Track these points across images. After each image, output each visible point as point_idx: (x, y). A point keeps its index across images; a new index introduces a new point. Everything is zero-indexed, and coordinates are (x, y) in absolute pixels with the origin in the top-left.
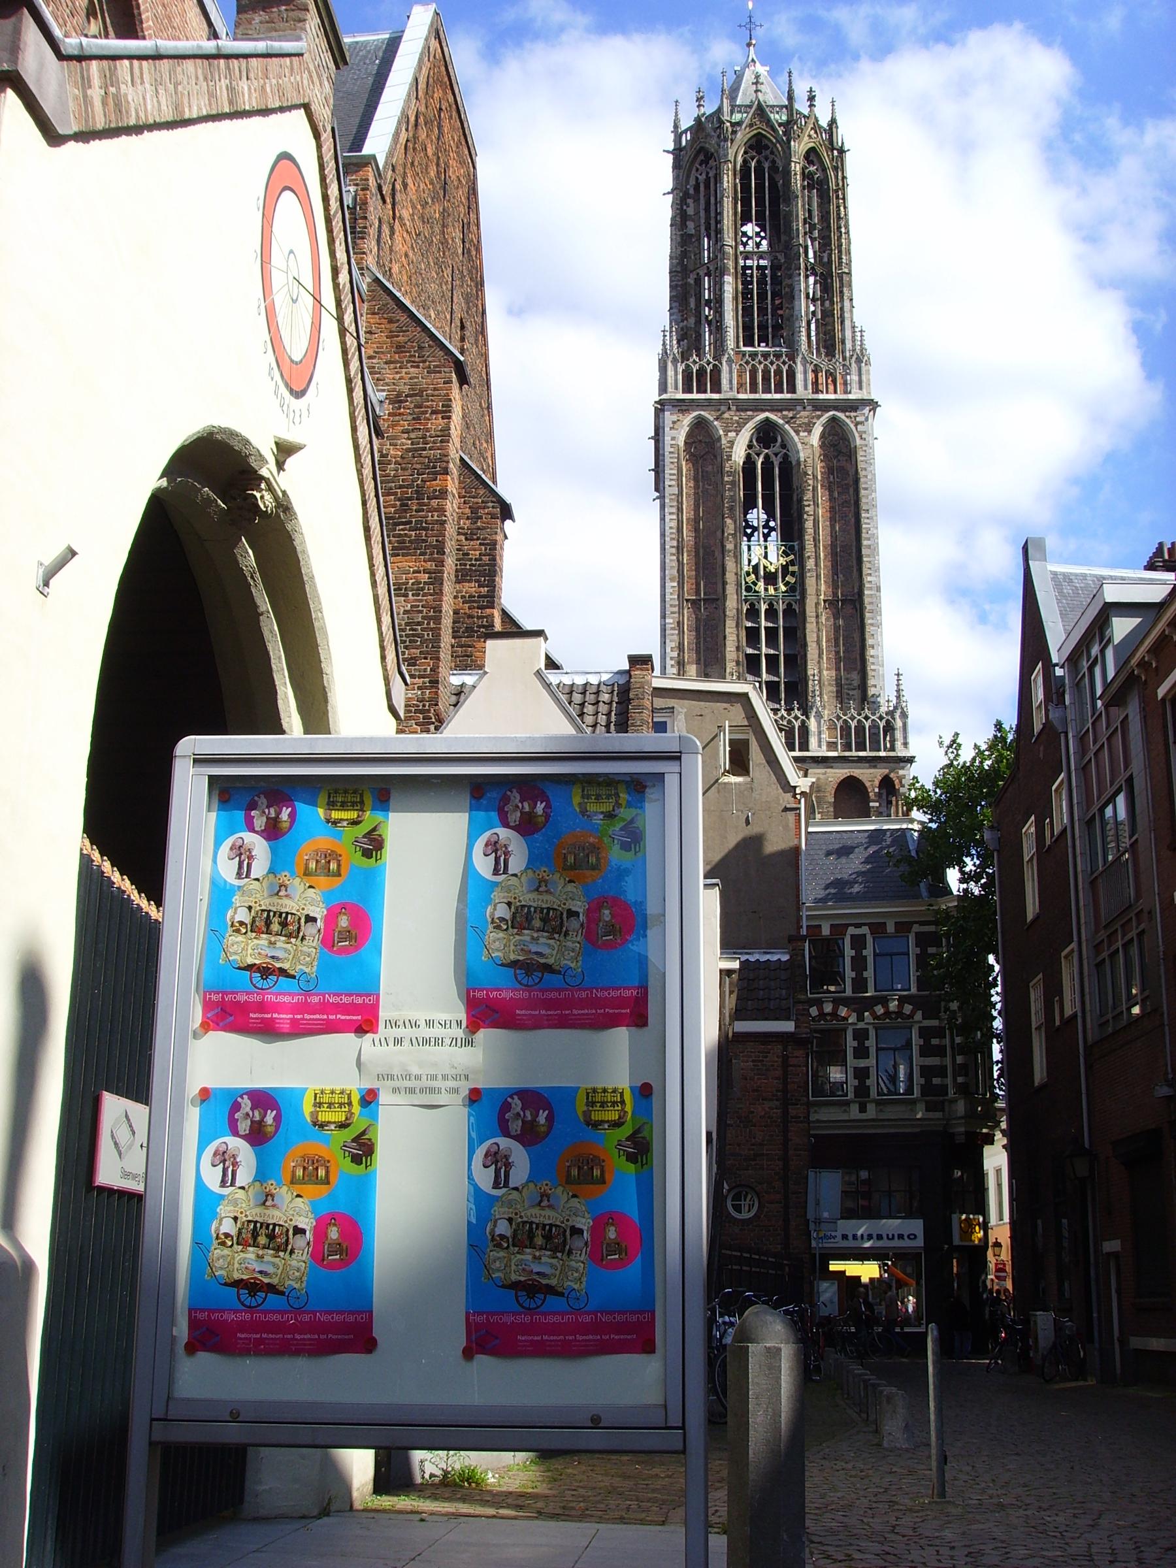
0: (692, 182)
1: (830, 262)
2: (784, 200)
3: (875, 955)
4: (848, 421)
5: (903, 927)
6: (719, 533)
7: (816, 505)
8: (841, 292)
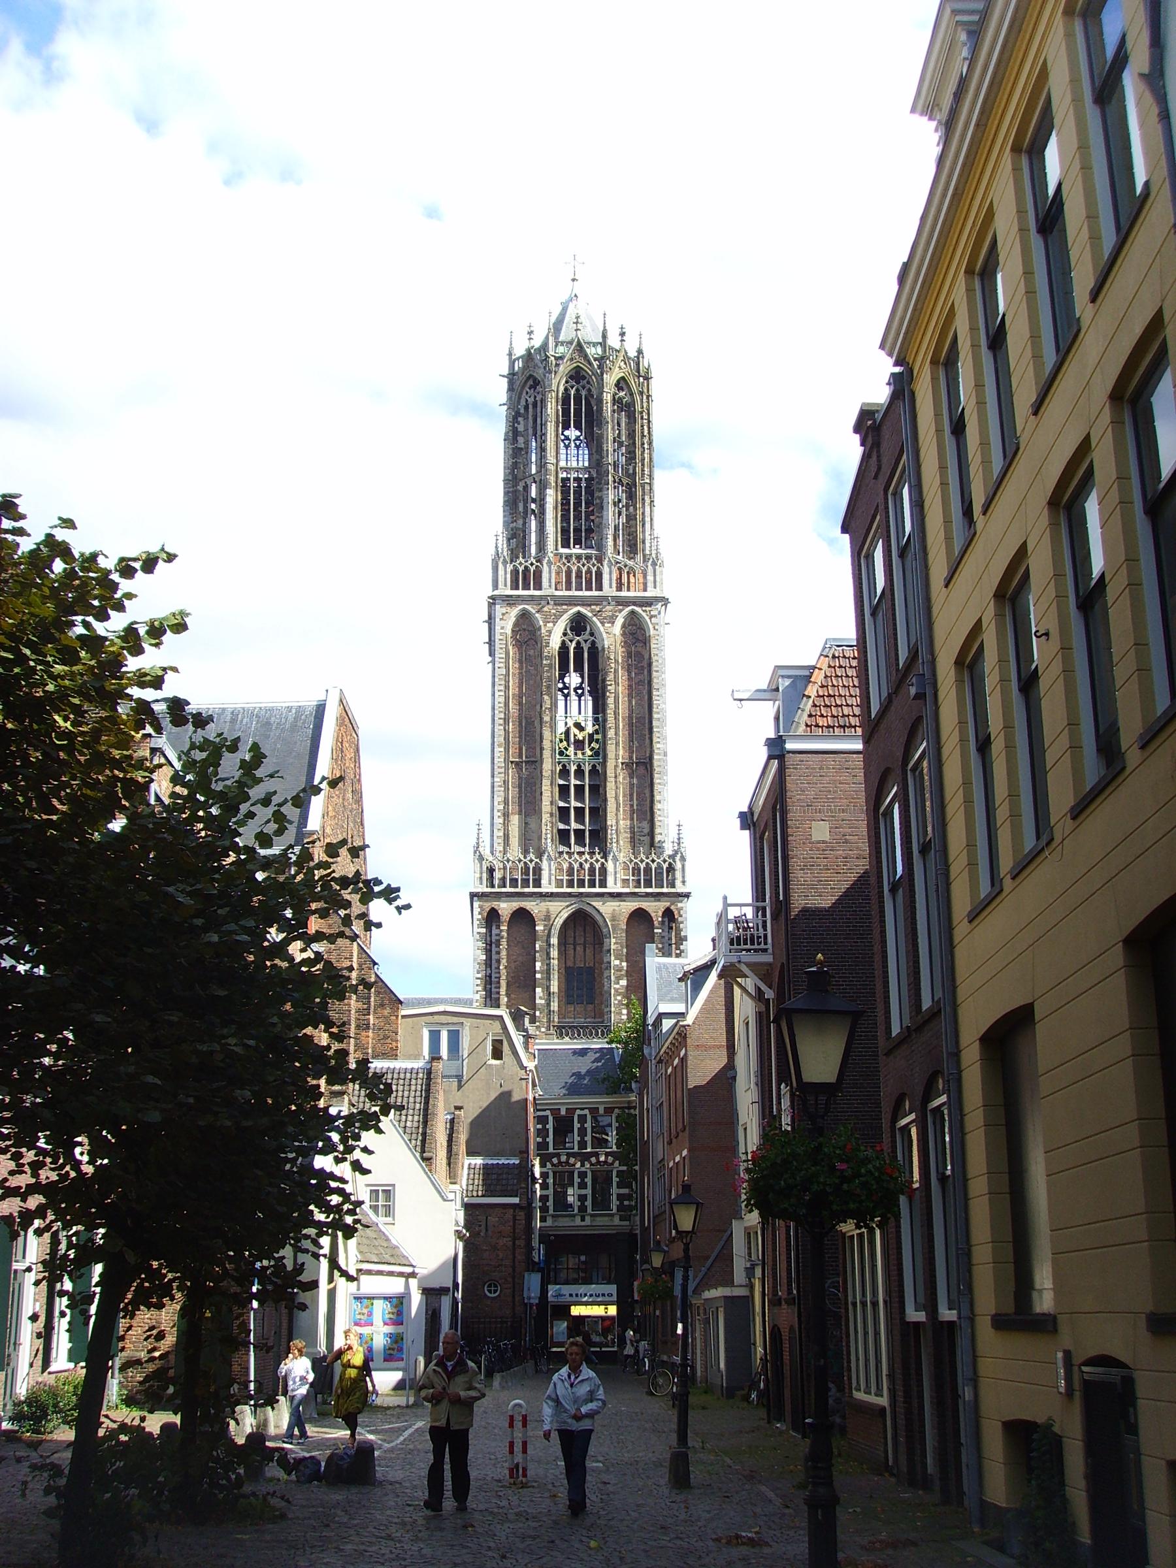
0: (523, 403)
1: (634, 472)
2: (597, 426)
3: (592, 1127)
4: (644, 614)
5: (609, 1111)
6: (538, 707)
7: (617, 684)
8: (643, 499)
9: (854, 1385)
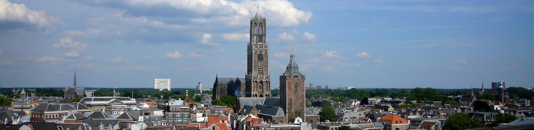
9: (501, 92)
